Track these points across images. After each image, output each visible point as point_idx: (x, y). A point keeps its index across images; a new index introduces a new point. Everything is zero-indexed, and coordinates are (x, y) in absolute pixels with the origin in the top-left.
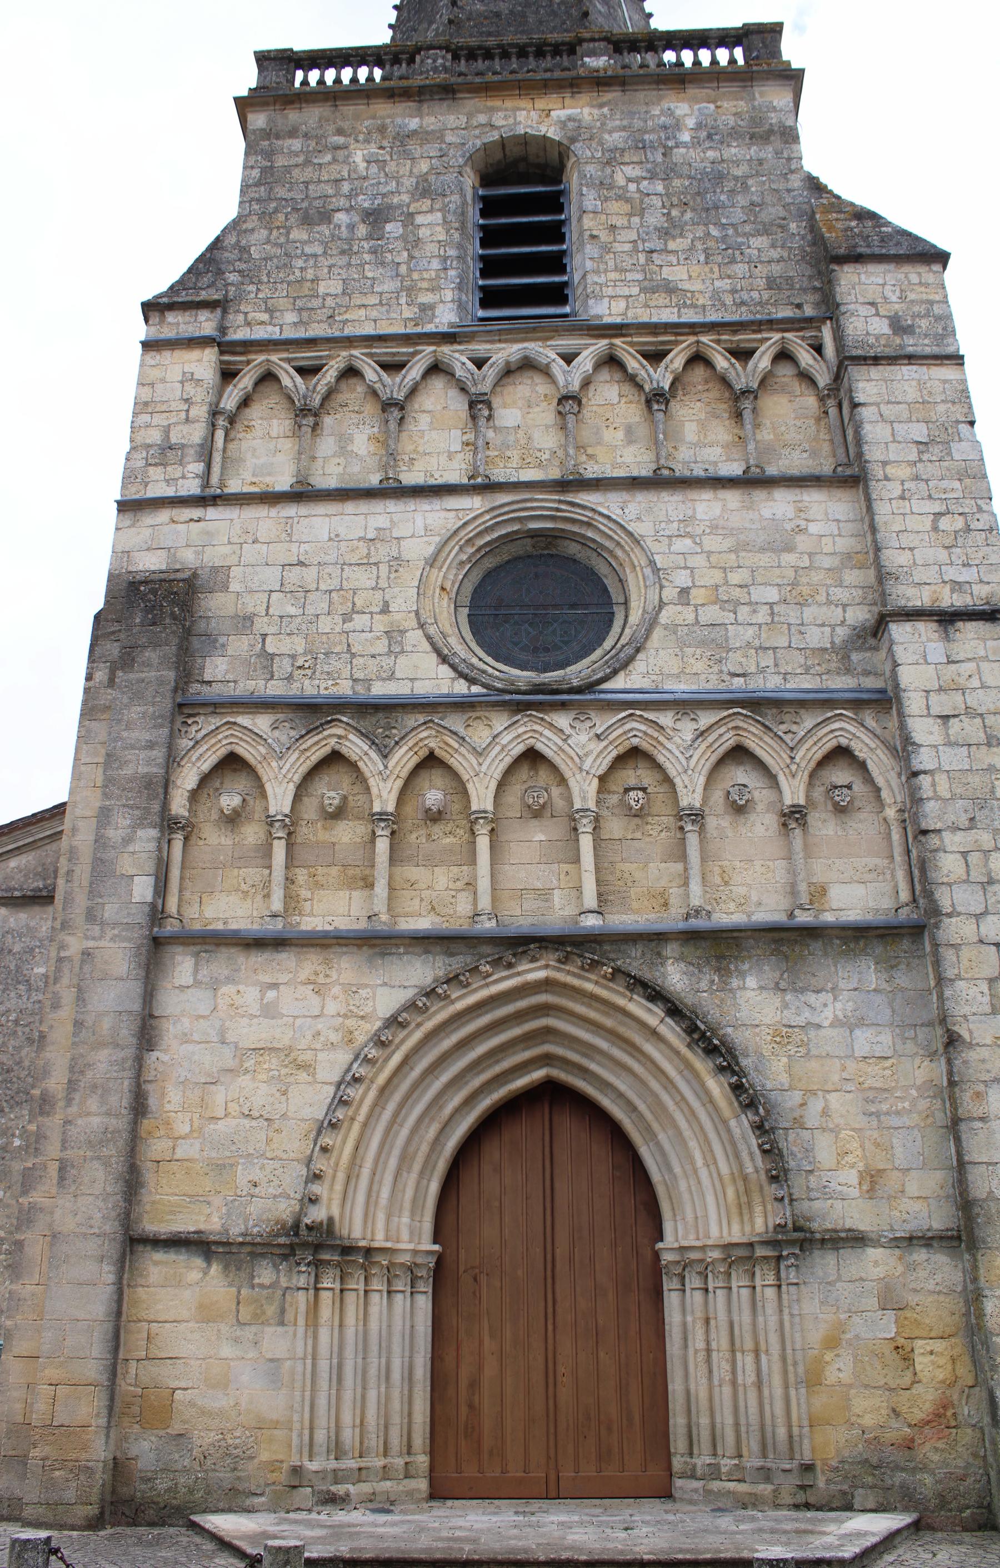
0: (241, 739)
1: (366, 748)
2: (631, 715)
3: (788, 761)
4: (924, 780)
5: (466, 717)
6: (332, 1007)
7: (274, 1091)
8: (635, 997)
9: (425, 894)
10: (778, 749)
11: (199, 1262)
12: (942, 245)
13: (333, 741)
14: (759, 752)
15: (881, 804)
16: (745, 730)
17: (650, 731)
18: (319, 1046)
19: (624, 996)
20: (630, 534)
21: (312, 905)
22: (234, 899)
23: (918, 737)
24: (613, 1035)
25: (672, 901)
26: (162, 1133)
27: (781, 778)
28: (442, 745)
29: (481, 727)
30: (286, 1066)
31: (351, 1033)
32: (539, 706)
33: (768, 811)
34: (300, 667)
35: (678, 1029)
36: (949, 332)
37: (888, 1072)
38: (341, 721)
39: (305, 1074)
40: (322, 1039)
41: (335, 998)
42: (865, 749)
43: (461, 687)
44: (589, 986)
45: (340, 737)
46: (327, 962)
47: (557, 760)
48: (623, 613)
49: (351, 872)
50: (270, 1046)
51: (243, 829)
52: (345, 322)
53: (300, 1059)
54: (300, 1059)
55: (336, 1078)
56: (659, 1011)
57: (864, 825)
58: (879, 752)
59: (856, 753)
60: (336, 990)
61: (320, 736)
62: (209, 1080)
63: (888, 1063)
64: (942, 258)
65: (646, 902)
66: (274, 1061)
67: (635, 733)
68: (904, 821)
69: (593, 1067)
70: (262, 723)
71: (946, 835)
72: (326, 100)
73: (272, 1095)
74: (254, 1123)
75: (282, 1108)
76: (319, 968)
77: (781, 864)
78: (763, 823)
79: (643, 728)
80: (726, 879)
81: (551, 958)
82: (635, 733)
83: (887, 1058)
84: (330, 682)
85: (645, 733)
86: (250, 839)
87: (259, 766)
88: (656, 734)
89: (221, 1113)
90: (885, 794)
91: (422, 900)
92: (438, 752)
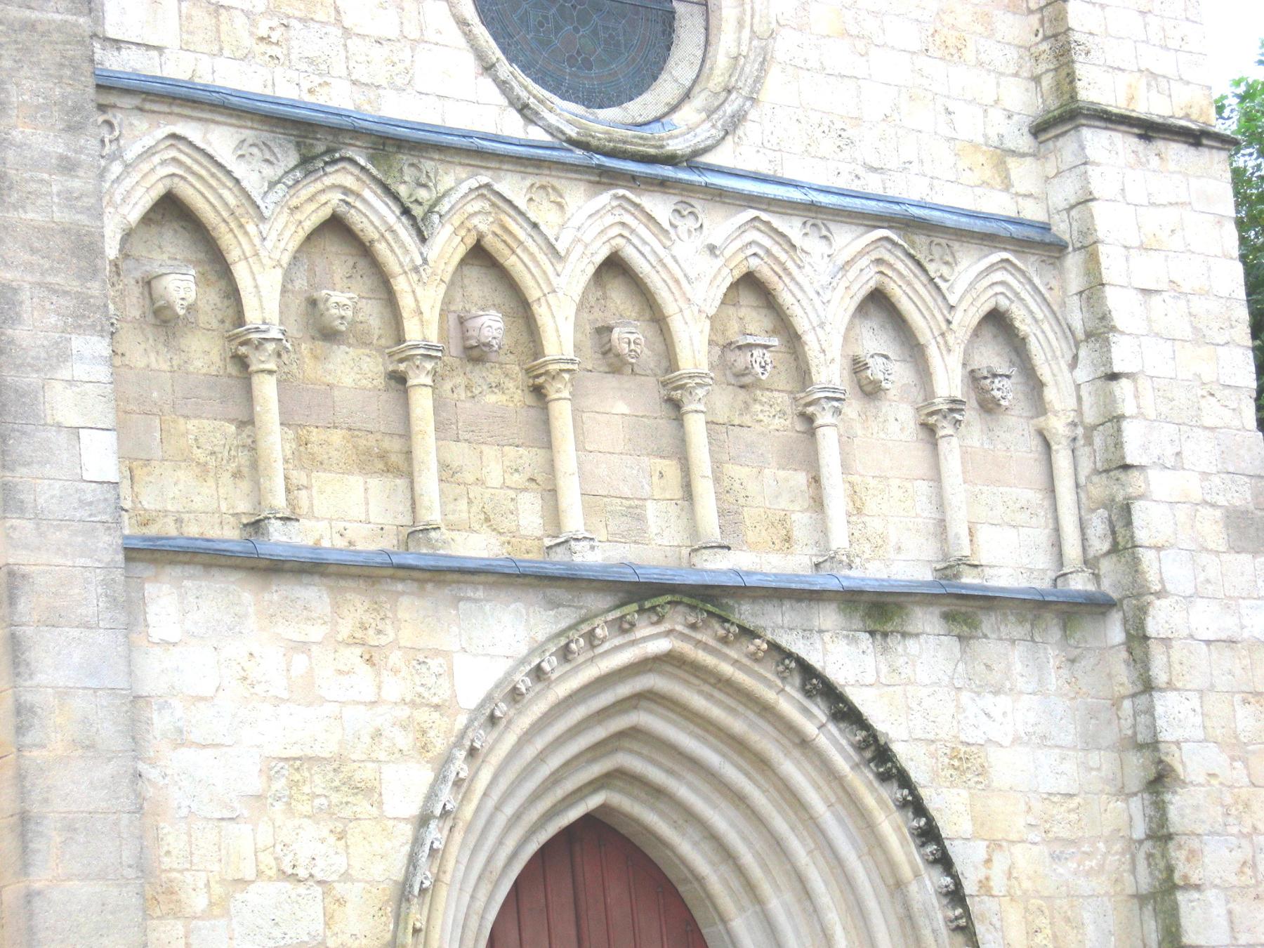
0: (189, 169)
1: (392, 219)
2: (756, 218)
3: (944, 326)
5: (528, 182)
6: (394, 688)
7: (325, 833)
8: (788, 688)
9: (475, 491)
10: (931, 304)
13: (335, 197)
14: (905, 306)
16: (895, 270)
17: (776, 250)
18: (382, 756)
19: (770, 685)
21: (310, 498)
22: (185, 476)
23: (1118, 320)
24: (737, 745)
25: (797, 534)
26: (165, 908)
27: (933, 352)
28: (499, 232)
29: (546, 204)
30: (337, 789)
31: (424, 733)
32: (633, 180)
33: (902, 399)
34: (262, 39)
35: (844, 742)
37: (1073, 817)
38: (351, 161)
39: (366, 804)
40: (385, 743)
41: (396, 671)
42: (1029, 320)
43: (513, 126)
44: (727, 669)
45: (346, 191)
46: (376, 607)
47: (655, 281)
48: (699, 22)
50: (310, 753)
51: (183, 343)
53: (357, 777)
54: (357, 777)
55: (414, 809)
56: (820, 711)
57: (1015, 434)
58: (1046, 327)
59: (1017, 324)
60: (395, 658)
61: (319, 186)
62: (227, 814)
63: (1073, 803)
65: (764, 533)
66: (318, 779)
67: (755, 249)
68: (1074, 439)
69: (683, 792)
70: (221, 140)
71: (1152, 474)
73: (323, 841)
74: (301, 889)
75: (340, 863)
76: (367, 618)
77: (923, 487)
78: (899, 416)
79: (767, 242)
80: (858, 504)
81: (677, 620)
82: (755, 249)
83: (1071, 796)
84: (318, 80)
85: (768, 251)
86: (198, 364)
87: (223, 228)
88: (783, 257)
89: (249, 874)
90: (1050, 394)
91: (470, 502)
92: (490, 242)
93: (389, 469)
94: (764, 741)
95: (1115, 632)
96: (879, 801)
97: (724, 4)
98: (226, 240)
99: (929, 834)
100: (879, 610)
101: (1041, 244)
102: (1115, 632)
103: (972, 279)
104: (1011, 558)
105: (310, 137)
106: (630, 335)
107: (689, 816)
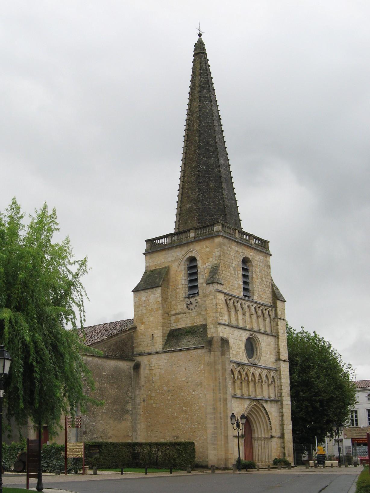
15: (275, 384)
94: (259, 411)
95: (280, 403)
96: (266, 416)
97: (354, 488)
99: (269, 419)
100: (266, 401)
101: (276, 371)
102: (280, 403)
103: (272, 373)
104: (272, 396)
106: (253, 379)
107: (252, 416)
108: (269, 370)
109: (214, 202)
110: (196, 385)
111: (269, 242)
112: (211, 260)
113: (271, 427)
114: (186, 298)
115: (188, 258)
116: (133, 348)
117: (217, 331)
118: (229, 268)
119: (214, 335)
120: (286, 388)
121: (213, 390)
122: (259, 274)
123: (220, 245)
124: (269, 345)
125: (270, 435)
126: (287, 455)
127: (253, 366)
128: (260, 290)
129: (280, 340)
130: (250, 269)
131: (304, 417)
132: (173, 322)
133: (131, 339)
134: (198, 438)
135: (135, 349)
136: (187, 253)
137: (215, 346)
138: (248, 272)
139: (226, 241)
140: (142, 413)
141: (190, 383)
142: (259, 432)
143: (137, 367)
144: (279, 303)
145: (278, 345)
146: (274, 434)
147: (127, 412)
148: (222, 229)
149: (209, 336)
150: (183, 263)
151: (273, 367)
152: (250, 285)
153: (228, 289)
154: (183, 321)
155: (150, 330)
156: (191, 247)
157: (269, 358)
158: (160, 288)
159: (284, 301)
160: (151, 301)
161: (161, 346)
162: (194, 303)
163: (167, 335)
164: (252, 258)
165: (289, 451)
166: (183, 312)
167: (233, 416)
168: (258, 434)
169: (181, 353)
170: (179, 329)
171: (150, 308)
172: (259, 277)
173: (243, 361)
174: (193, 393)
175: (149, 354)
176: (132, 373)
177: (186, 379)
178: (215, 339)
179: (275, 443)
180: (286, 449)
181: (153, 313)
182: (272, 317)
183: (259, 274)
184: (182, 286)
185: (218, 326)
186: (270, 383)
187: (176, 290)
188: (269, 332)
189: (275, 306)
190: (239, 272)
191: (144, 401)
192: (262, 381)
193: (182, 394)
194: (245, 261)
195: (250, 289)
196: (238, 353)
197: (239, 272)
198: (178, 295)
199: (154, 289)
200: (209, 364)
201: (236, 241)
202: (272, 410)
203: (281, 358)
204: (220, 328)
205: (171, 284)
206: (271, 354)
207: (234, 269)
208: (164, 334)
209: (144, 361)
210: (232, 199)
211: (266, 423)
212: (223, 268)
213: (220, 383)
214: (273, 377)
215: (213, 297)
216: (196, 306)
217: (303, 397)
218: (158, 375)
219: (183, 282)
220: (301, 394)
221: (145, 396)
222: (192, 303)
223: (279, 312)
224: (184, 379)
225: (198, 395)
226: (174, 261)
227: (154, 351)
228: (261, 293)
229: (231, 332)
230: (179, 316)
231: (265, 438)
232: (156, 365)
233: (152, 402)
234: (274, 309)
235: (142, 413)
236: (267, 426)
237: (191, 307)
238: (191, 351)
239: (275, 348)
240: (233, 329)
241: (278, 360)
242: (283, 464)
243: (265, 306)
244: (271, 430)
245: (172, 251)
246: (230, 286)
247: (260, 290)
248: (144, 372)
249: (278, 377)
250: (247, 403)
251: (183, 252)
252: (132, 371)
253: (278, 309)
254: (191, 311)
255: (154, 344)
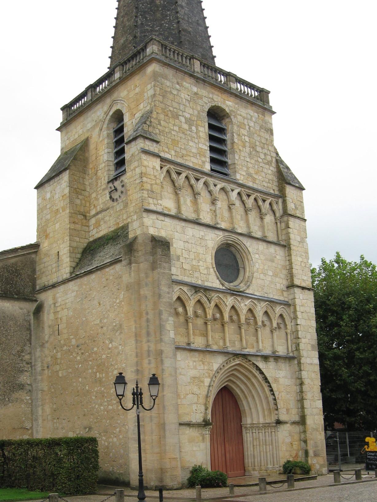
4: (299, 326)
6: (206, 368)
11: (188, 428)
12: (304, 186)
15: (286, 328)
20: (248, 251)
36: (303, 212)
47: (238, 309)
49: (201, 332)
52: (186, 160)
60: (206, 363)
64: (304, 189)
72: (174, 69)
81: (240, 359)
90: (288, 327)
93: (204, 336)
94: (250, 376)
95: (296, 362)
96: (265, 385)
98: (186, 303)
99: (272, 390)
100: (265, 358)
102: (296, 362)
103: (278, 310)
104: (281, 350)
105: (196, 288)
106: (235, 318)
107: (238, 386)
108: (272, 302)
109: (161, 25)
110: (113, 330)
111: (268, 92)
112: (141, 106)
113: (276, 404)
114: (108, 182)
115: (112, 116)
116: (33, 281)
117: (142, 225)
118: (176, 117)
119: (138, 232)
120: (309, 336)
121: (136, 336)
122: (247, 139)
123: (155, 76)
124: (272, 261)
125: (273, 419)
126: (311, 453)
127: (233, 295)
128: (250, 165)
129: (293, 253)
130: (229, 128)
131: (363, 389)
132: (92, 228)
133: (32, 266)
134: (118, 430)
135: (38, 282)
136: (111, 107)
137: (140, 253)
138: (225, 134)
139: (169, 72)
140: (46, 388)
141: (105, 328)
142: (255, 414)
143: (39, 310)
144: (290, 191)
145: (290, 261)
146: (283, 417)
147: (21, 387)
148: (159, 50)
149: (131, 236)
150: (105, 126)
151: (282, 298)
152: (230, 156)
153: (173, 153)
154: (105, 222)
155: (54, 245)
156: (115, 95)
157: (271, 282)
158: (68, 171)
159: (302, 189)
160: (57, 196)
161: (68, 270)
162: (119, 188)
163: (81, 250)
164: (231, 111)
165: (316, 446)
166: (105, 208)
167: (120, 380)
168: (252, 419)
169: (93, 276)
170: (99, 238)
171: (55, 208)
172: (247, 144)
173: (208, 284)
174: (110, 346)
175: (54, 286)
176: (32, 321)
177: (101, 321)
178: (140, 240)
179: (285, 435)
180: (310, 443)
181: (59, 215)
182: (278, 215)
183: (247, 139)
184: (103, 165)
185: (145, 215)
186: (275, 325)
187: (96, 174)
188: (271, 236)
189: (282, 195)
190: (201, 129)
191: (48, 367)
192: (256, 323)
193: (95, 349)
194: (216, 115)
195: (229, 162)
196: (195, 269)
197: (201, 129)
198: (99, 181)
199: (61, 176)
200: (128, 287)
201: (191, 76)
202: (279, 375)
203: (297, 282)
204: (149, 220)
205: (91, 166)
206: (275, 275)
207: (189, 122)
208: (77, 248)
209: (47, 298)
210: (198, 24)
211: (267, 398)
212: (162, 116)
213: (148, 321)
214: (281, 316)
215: (136, 164)
216: (122, 192)
217: (361, 359)
218: (64, 318)
219: (105, 157)
220: (357, 353)
221: (49, 359)
222: (116, 190)
223: (291, 206)
224: (98, 322)
225: (116, 348)
226: (95, 128)
227: (60, 279)
228: (252, 171)
229: (179, 228)
230: (100, 216)
231: (266, 426)
232: (63, 303)
233: (58, 367)
234: (280, 201)
235: (46, 388)
236: (268, 402)
237: (115, 195)
238: (107, 270)
239: (284, 267)
240: (183, 224)
241: (291, 286)
242: (299, 471)
243: (260, 192)
244: (277, 409)
245: (92, 111)
246: (178, 150)
247: (250, 165)
248: (48, 317)
249: (292, 316)
250: (217, 362)
251: (106, 108)
252: (32, 317)
253: (289, 199)
254: (115, 204)
255: (60, 268)
